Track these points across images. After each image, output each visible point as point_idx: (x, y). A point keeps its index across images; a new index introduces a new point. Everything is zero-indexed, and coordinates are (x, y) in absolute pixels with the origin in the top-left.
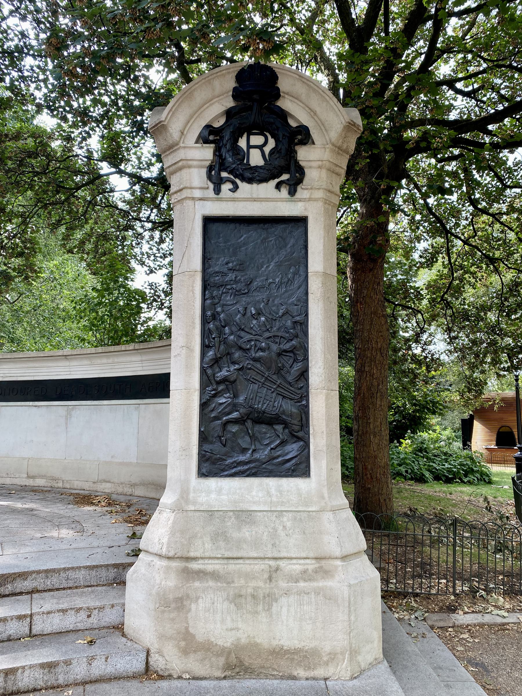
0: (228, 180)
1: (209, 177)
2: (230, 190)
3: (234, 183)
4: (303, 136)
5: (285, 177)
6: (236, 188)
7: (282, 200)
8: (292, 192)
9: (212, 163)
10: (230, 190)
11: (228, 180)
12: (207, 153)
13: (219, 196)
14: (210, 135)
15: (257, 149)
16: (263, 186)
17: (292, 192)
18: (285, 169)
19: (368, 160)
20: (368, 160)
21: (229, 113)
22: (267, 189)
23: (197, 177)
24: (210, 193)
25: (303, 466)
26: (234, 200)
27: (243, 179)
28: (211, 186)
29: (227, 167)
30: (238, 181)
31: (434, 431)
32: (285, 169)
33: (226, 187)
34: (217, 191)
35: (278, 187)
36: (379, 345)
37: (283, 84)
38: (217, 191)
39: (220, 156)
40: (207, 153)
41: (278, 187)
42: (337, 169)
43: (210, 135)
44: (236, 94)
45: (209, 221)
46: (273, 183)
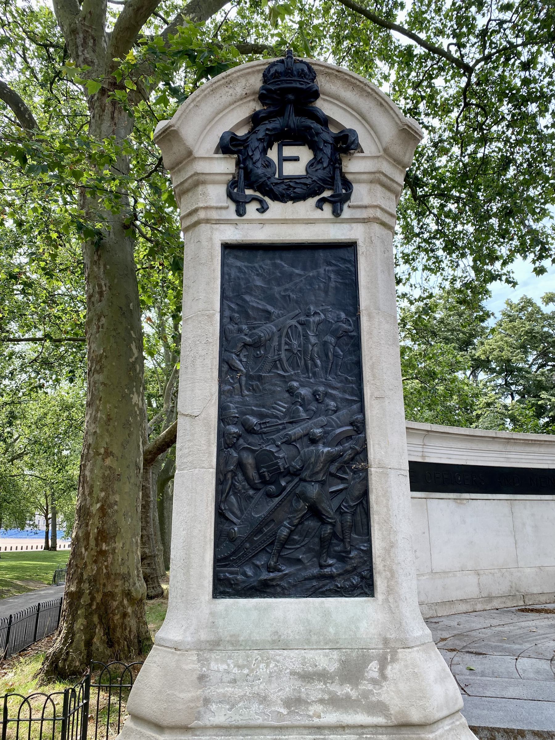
0: (254, 199)
1: (230, 195)
2: (257, 210)
3: (261, 201)
4: (346, 143)
5: (327, 194)
6: (263, 209)
7: (325, 221)
8: (337, 213)
9: (234, 178)
10: (257, 210)
11: (254, 199)
12: (226, 166)
13: (244, 217)
14: (229, 145)
15: (296, 161)
16: (300, 205)
17: (337, 213)
18: (330, 186)
19: (209, 76)
20: (209, 76)
21: (255, 120)
22: (306, 208)
23: (216, 194)
24: (231, 213)
25: (361, 456)
26: (263, 222)
27: (275, 197)
28: (233, 207)
29: (253, 184)
30: (267, 199)
31: (486, 394)
32: (330, 186)
33: (252, 209)
34: (240, 212)
35: (319, 205)
36: (404, 191)
37: (323, 83)
38: (240, 212)
39: (245, 169)
40: (226, 166)
41: (319, 205)
42: (403, 472)
43: (229, 145)
44: (263, 96)
45: (227, 247)
46: (312, 201)
